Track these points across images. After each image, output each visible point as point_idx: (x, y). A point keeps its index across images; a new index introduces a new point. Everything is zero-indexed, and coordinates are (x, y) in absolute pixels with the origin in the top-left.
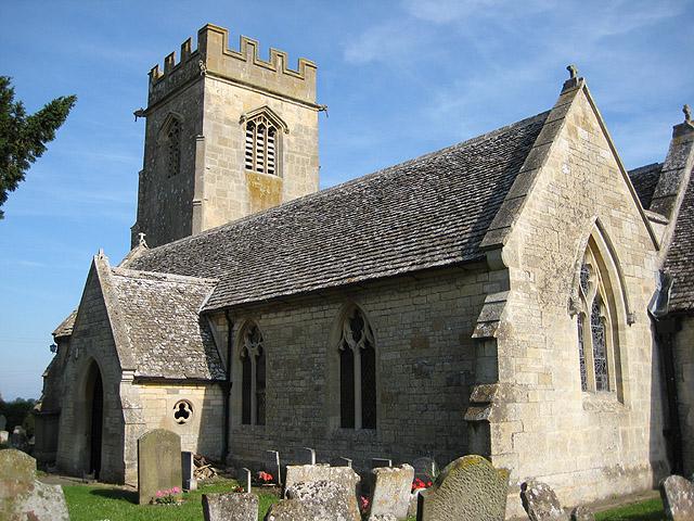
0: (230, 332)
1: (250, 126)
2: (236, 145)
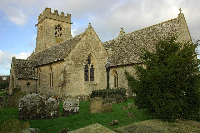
0: (37, 70)
1: (56, 28)
2: (53, 32)
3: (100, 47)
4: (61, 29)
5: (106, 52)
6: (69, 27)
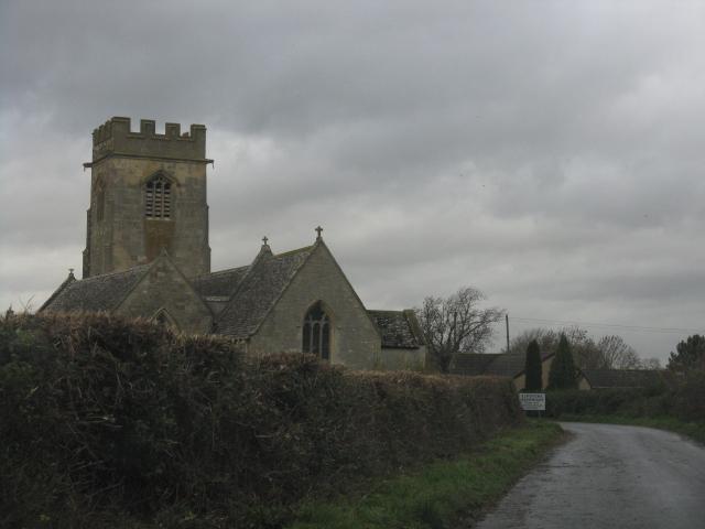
1: (150, 185)
4: (167, 186)
5: (204, 308)
6: (196, 175)
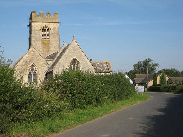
1: (43, 30)
3: (40, 60)
